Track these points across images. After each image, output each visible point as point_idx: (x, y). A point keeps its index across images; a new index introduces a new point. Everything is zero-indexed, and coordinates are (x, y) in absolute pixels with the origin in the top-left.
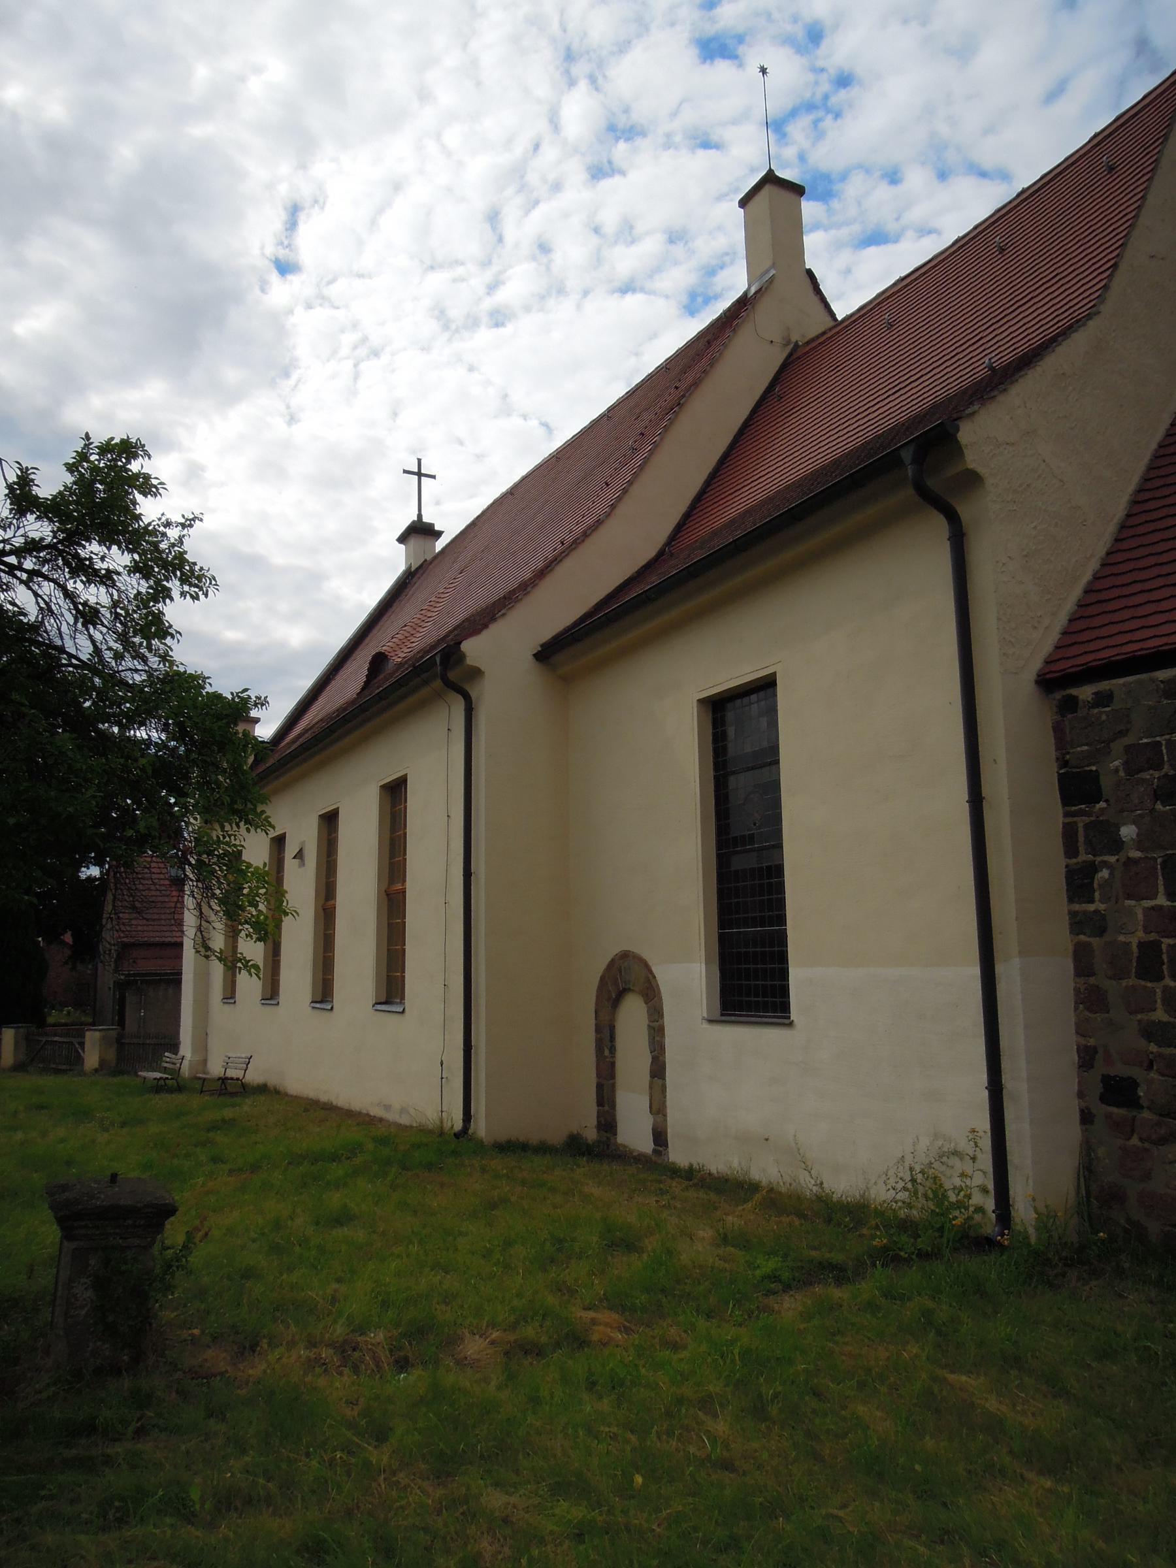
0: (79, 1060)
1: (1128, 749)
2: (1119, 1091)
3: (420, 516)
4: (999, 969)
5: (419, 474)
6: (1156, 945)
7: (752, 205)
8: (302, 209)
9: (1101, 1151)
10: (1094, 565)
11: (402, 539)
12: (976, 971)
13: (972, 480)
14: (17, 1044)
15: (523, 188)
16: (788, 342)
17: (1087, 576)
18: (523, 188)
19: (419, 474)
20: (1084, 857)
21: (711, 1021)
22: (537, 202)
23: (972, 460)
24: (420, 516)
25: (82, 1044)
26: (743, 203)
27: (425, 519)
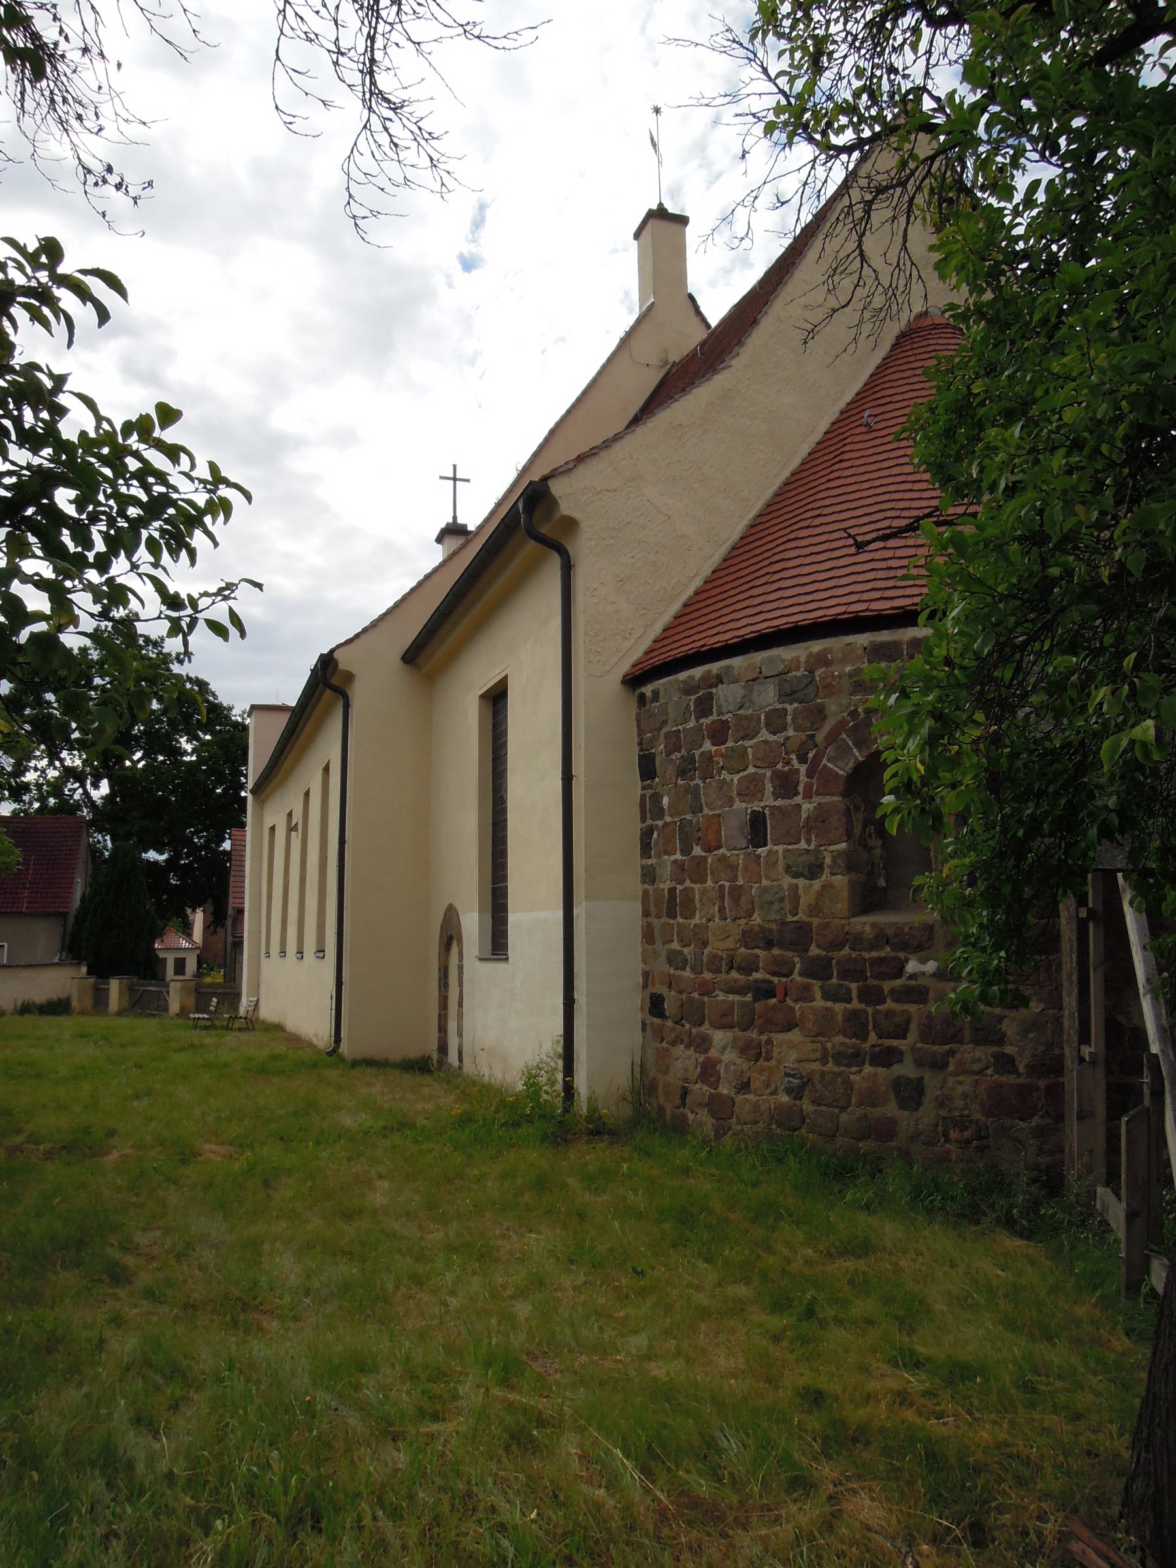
0: (166, 1009)
1: (667, 735)
2: (656, 1005)
3: (455, 518)
4: (515, 918)
5: (455, 479)
6: (675, 888)
7: (642, 237)
8: (488, 206)
9: (650, 1051)
10: (697, 583)
11: (439, 540)
12: (560, 914)
13: (570, 524)
14: (121, 993)
15: (705, 164)
16: (666, 363)
17: (690, 592)
18: (705, 164)
19: (455, 479)
20: (649, 822)
21: (481, 959)
22: (718, 176)
23: (566, 508)
24: (455, 518)
25: (168, 992)
26: (637, 236)
27: (460, 521)
